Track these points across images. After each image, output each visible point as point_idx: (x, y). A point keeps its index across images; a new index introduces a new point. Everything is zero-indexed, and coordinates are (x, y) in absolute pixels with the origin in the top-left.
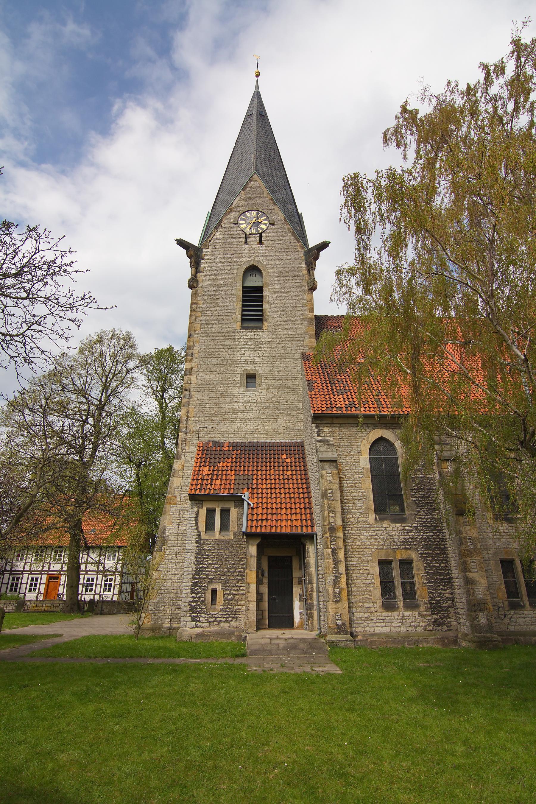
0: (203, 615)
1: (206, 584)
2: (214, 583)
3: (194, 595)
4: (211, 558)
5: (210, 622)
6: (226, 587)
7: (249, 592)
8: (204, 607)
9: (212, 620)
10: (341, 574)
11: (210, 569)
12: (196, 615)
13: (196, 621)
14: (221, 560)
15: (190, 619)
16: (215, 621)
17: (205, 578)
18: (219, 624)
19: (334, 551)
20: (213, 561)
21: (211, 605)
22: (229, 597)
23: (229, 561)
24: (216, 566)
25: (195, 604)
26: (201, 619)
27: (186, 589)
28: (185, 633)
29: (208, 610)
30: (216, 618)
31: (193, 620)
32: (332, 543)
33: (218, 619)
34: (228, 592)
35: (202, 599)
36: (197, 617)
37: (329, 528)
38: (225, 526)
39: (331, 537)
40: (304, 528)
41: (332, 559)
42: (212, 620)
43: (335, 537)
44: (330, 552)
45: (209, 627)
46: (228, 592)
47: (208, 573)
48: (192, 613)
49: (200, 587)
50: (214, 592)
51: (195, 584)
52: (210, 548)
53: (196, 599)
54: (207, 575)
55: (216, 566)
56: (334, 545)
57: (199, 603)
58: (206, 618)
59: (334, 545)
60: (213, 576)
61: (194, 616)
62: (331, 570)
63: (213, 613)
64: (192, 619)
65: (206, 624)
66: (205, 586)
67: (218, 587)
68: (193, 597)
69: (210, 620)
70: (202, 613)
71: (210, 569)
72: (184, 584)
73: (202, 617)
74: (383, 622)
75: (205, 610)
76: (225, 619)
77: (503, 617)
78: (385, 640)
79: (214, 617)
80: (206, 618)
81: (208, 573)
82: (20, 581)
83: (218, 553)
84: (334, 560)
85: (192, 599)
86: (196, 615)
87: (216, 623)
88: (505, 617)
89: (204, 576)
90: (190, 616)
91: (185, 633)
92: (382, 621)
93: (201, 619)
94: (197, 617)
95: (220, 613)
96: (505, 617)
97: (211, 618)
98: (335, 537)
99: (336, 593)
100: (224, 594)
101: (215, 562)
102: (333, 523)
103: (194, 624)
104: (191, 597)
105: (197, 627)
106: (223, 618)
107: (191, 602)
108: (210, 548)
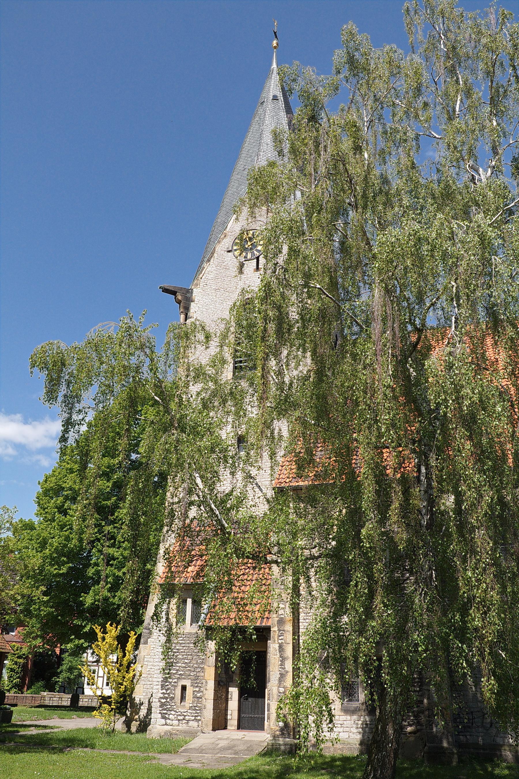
0: (173, 712)
1: (176, 680)
2: (184, 679)
3: (164, 691)
4: (182, 652)
5: (179, 720)
6: (196, 683)
7: (206, 690)
8: (173, 704)
9: (181, 718)
10: (287, 672)
11: (180, 664)
12: (165, 712)
13: (165, 718)
14: (191, 655)
15: (160, 716)
16: (184, 719)
17: (175, 674)
18: (187, 723)
19: (281, 646)
20: (183, 655)
21: (181, 702)
22: (199, 695)
23: (199, 656)
24: (186, 661)
25: (165, 700)
26: (171, 716)
27: (157, 685)
28: (154, 730)
29: (177, 707)
30: (185, 716)
31: (163, 717)
32: (280, 638)
33: (186, 717)
34: (197, 689)
35: (171, 695)
36: (166, 714)
37: (278, 621)
38: (195, 618)
39: (279, 630)
40: (265, 619)
41: (278, 656)
42: (181, 718)
43: (284, 631)
44: (277, 648)
45: (178, 725)
46: (197, 689)
47: (178, 668)
48: (162, 710)
49: (170, 683)
50: (184, 688)
51: (165, 680)
52: (181, 642)
53: (166, 695)
54: (177, 670)
55: (186, 661)
56: (282, 639)
57: (168, 700)
58: (176, 716)
59: (282, 639)
60: (183, 671)
61: (164, 713)
62: (277, 667)
63: (182, 711)
64: (162, 716)
65: (176, 722)
66: (175, 682)
67: (187, 683)
68: (163, 693)
69: (179, 718)
70: (171, 711)
71: (180, 664)
72: (154, 680)
73: (171, 714)
74: (341, 727)
75: (175, 707)
76: (193, 718)
77: (489, 726)
78: (341, 747)
79: (183, 715)
80: (176, 716)
81: (178, 668)
82: (96, 673)
83: (189, 647)
84: (280, 657)
85: (162, 696)
86: (165, 712)
87: (184, 721)
88: (491, 726)
89: (174, 672)
90: (160, 713)
91: (154, 730)
92: (339, 725)
93: (171, 716)
94: (166, 714)
95: (189, 711)
96: (491, 726)
97: (180, 715)
98: (284, 631)
99: (280, 693)
100: (193, 692)
101: (185, 656)
102: (282, 615)
103: (163, 721)
104: (162, 693)
105: (166, 724)
106: (192, 716)
107: (161, 698)
108: (181, 642)
